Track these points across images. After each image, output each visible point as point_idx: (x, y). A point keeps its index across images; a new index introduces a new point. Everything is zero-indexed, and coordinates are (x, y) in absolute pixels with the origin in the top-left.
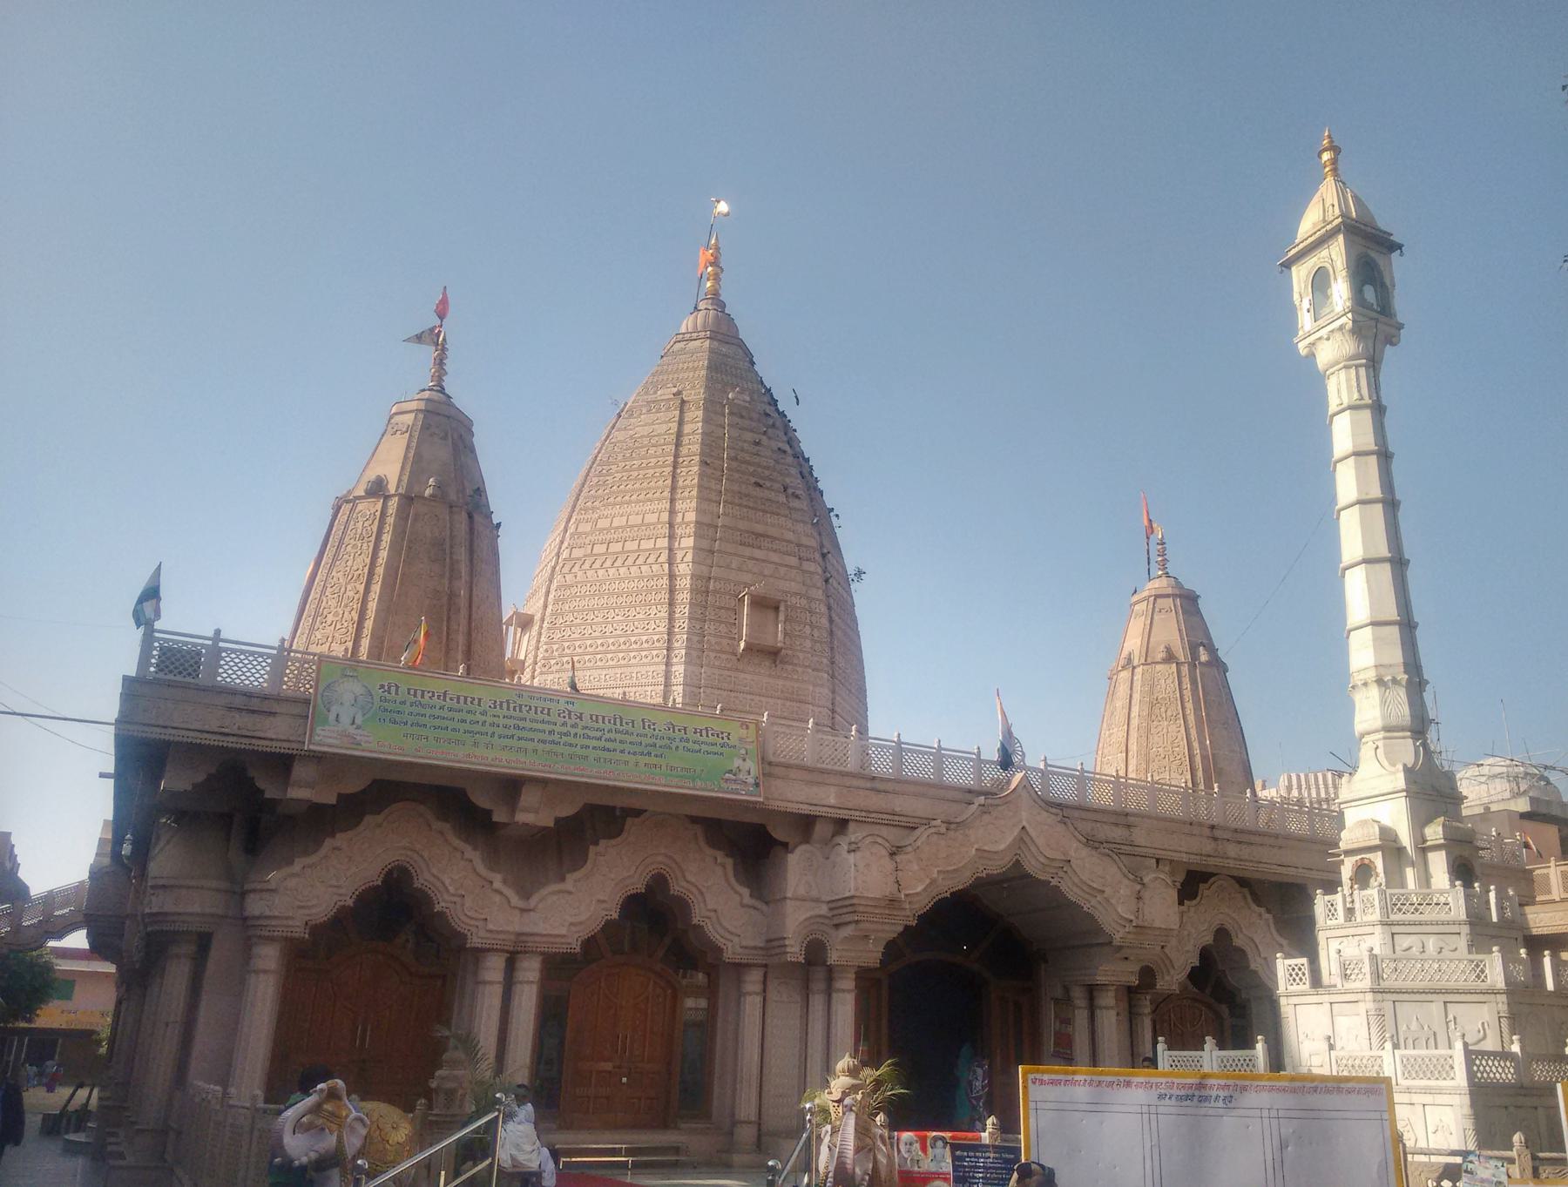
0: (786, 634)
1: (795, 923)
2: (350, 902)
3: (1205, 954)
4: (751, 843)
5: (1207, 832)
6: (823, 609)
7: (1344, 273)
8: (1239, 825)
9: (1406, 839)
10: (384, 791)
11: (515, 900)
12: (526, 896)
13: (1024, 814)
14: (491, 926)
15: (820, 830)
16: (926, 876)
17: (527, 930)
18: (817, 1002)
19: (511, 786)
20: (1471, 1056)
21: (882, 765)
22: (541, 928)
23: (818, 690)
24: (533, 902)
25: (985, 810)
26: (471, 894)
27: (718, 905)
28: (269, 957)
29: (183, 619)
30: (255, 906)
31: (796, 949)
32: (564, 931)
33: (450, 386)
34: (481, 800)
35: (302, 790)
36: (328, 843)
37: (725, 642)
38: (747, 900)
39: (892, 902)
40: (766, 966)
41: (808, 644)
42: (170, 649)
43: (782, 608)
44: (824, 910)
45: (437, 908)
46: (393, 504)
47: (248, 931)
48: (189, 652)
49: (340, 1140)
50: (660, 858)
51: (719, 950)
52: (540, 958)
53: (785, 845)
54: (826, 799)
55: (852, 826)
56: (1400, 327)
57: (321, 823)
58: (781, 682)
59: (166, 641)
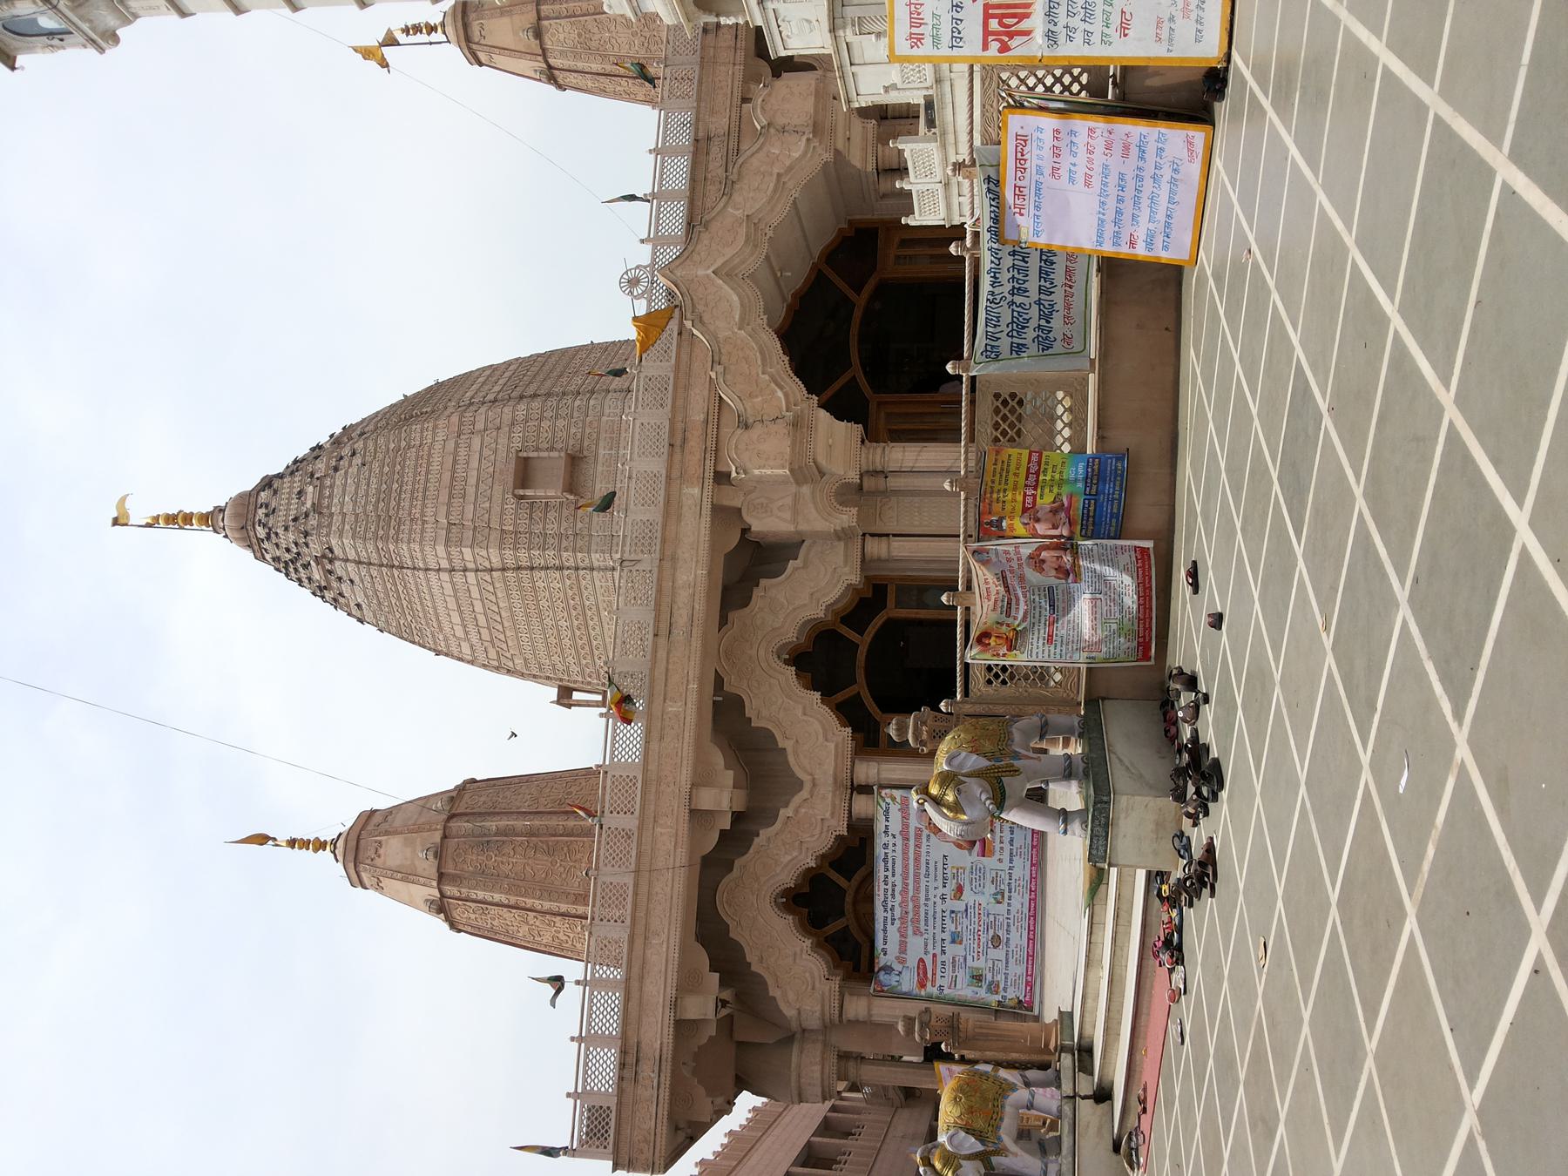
0: (552, 449)
2: (808, 942)
4: (750, 562)
5: (711, 36)
11: (804, 794)
12: (800, 785)
13: (701, 272)
14: (828, 815)
15: (732, 499)
16: (768, 384)
17: (831, 780)
18: (894, 483)
19: (698, 816)
22: (829, 767)
23: (607, 411)
25: (699, 321)
27: (810, 592)
29: (561, 1126)
30: (813, 1022)
31: (845, 517)
32: (832, 746)
33: (328, 835)
37: (565, 512)
39: (797, 424)
41: (561, 423)
44: (806, 490)
46: (450, 890)
47: (838, 1023)
49: (970, 1157)
50: (762, 652)
54: (695, 496)
55: (721, 468)
58: (601, 452)
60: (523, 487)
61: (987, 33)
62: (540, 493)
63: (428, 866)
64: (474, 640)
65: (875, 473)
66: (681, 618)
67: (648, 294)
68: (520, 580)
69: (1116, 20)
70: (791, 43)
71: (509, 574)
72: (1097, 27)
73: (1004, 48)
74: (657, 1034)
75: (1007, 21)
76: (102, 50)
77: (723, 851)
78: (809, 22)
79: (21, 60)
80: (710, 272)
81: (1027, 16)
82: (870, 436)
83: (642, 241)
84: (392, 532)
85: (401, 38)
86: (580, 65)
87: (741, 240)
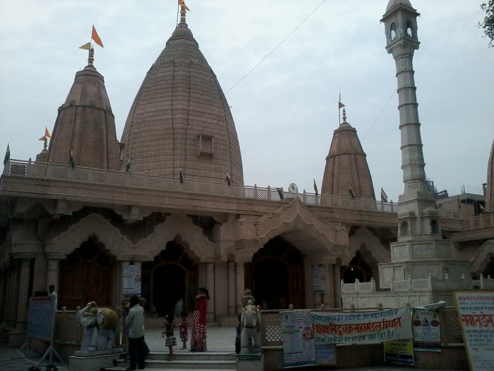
1: (224, 249)
3: (358, 253)
4: (208, 224)
6: (227, 139)
7: (401, 25)
8: (370, 210)
9: (417, 214)
10: (87, 210)
13: (298, 210)
14: (125, 253)
15: (231, 218)
18: (232, 273)
19: (128, 208)
20: (433, 280)
21: (249, 195)
24: (137, 245)
26: (115, 242)
27: (198, 245)
28: (54, 266)
30: (48, 249)
33: (95, 64)
34: (119, 212)
35: (62, 210)
36: (70, 228)
38: (208, 241)
40: (214, 263)
42: (15, 165)
43: (213, 139)
44: (233, 244)
45: (107, 248)
47: (47, 258)
48: (21, 166)
49: (96, 320)
51: (115, 257)
52: (140, 263)
53: (219, 223)
55: (241, 216)
56: (419, 43)
57: (64, 222)
58: (213, 165)
59: (14, 163)
60: (202, 138)
61: (466, 316)
62: (201, 143)
63: (87, 103)
64: (145, 115)
65: (235, 267)
66: (195, 203)
67: (290, 192)
68: (191, 129)
69: (476, 347)
70: (395, 249)
71: (171, 131)
72: (473, 343)
73: (463, 320)
74: (54, 192)
75: (470, 321)
76: (386, 48)
77: (111, 215)
78: (402, 254)
79: (383, 24)
80: (298, 213)
81: (472, 326)
82: (246, 265)
83: (304, 191)
84: (185, 89)
85: (342, 109)
86: (336, 166)
87: (307, 223)
